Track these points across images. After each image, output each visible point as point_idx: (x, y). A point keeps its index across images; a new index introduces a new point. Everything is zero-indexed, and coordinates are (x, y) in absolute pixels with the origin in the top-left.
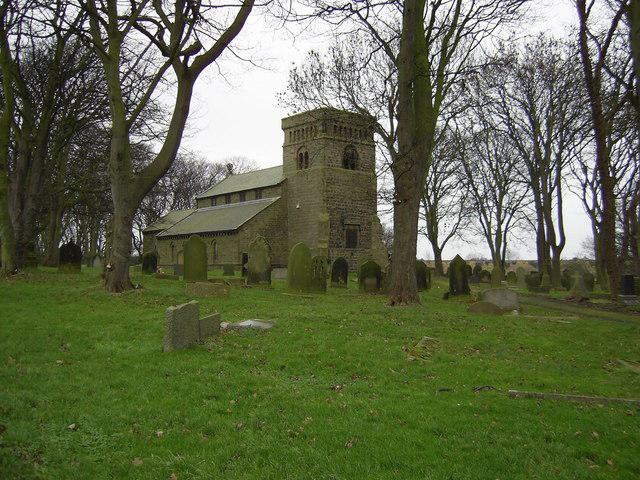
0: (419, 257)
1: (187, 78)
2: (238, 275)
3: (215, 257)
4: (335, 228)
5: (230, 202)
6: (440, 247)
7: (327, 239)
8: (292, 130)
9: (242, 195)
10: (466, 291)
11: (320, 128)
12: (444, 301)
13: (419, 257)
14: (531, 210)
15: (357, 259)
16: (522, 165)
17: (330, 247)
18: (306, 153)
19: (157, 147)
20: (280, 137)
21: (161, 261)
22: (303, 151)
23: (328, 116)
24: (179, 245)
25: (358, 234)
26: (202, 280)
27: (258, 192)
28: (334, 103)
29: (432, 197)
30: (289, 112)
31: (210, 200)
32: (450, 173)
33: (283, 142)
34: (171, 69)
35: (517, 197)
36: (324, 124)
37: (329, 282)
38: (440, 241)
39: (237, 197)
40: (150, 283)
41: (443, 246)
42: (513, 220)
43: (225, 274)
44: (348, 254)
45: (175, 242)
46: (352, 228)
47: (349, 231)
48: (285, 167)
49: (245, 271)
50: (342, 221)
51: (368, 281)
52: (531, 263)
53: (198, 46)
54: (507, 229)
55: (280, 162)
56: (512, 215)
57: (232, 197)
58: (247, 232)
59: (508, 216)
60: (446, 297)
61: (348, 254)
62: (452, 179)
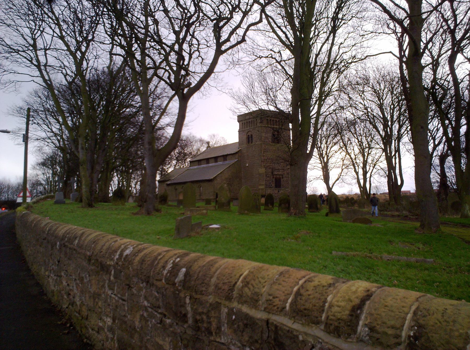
0: (309, 191)
1: (184, 100)
2: (213, 204)
3: (200, 196)
4: (268, 177)
5: (226, 160)
6: (331, 186)
7: (264, 183)
8: (246, 122)
9: (216, 159)
10: (338, 211)
11: (259, 121)
12: (326, 218)
13: (309, 191)
14: (383, 164)
15: (277, 194)
16: (377, 138)
17: (266, 187)
18: (252, 135)
19: (170, 131)
20: (236, 126)
21: (169, 198)
22: (249, 134)
23: (261, 113)
24: (179, 188)
25: (282, 180)
26: (194, 207)
27: (225, 157)
28: (265, 107)
29: (326, 158)
30: (244, 111)
31: (205, 161)
32: (335, 144)
33: (238, 128)
34: (176, 97)
35: (377, 157)
36: (261, 118)
37: (262, 207)
38: (331, 183)
39: (213, 160)
40: (164, 208)
41: (333, 186)
42: (375, 170)
43: (206, 204)
44: (276, 192)
45: (177, 187)
46: (278, 176)
47: (276, 179)
48: (240, 142)
49: (217, 201)
50: (272, 173)
51: (283, 205)
52: (384, 194)
53: (190, 84)
54: (371, 176)
55: (237, 140)
56: (374, 167)
57: (210, 160)
58: (219, 180)
59: (372, 168)
60: (327, 215)
61: (276, 192)
62: (336, 148)
